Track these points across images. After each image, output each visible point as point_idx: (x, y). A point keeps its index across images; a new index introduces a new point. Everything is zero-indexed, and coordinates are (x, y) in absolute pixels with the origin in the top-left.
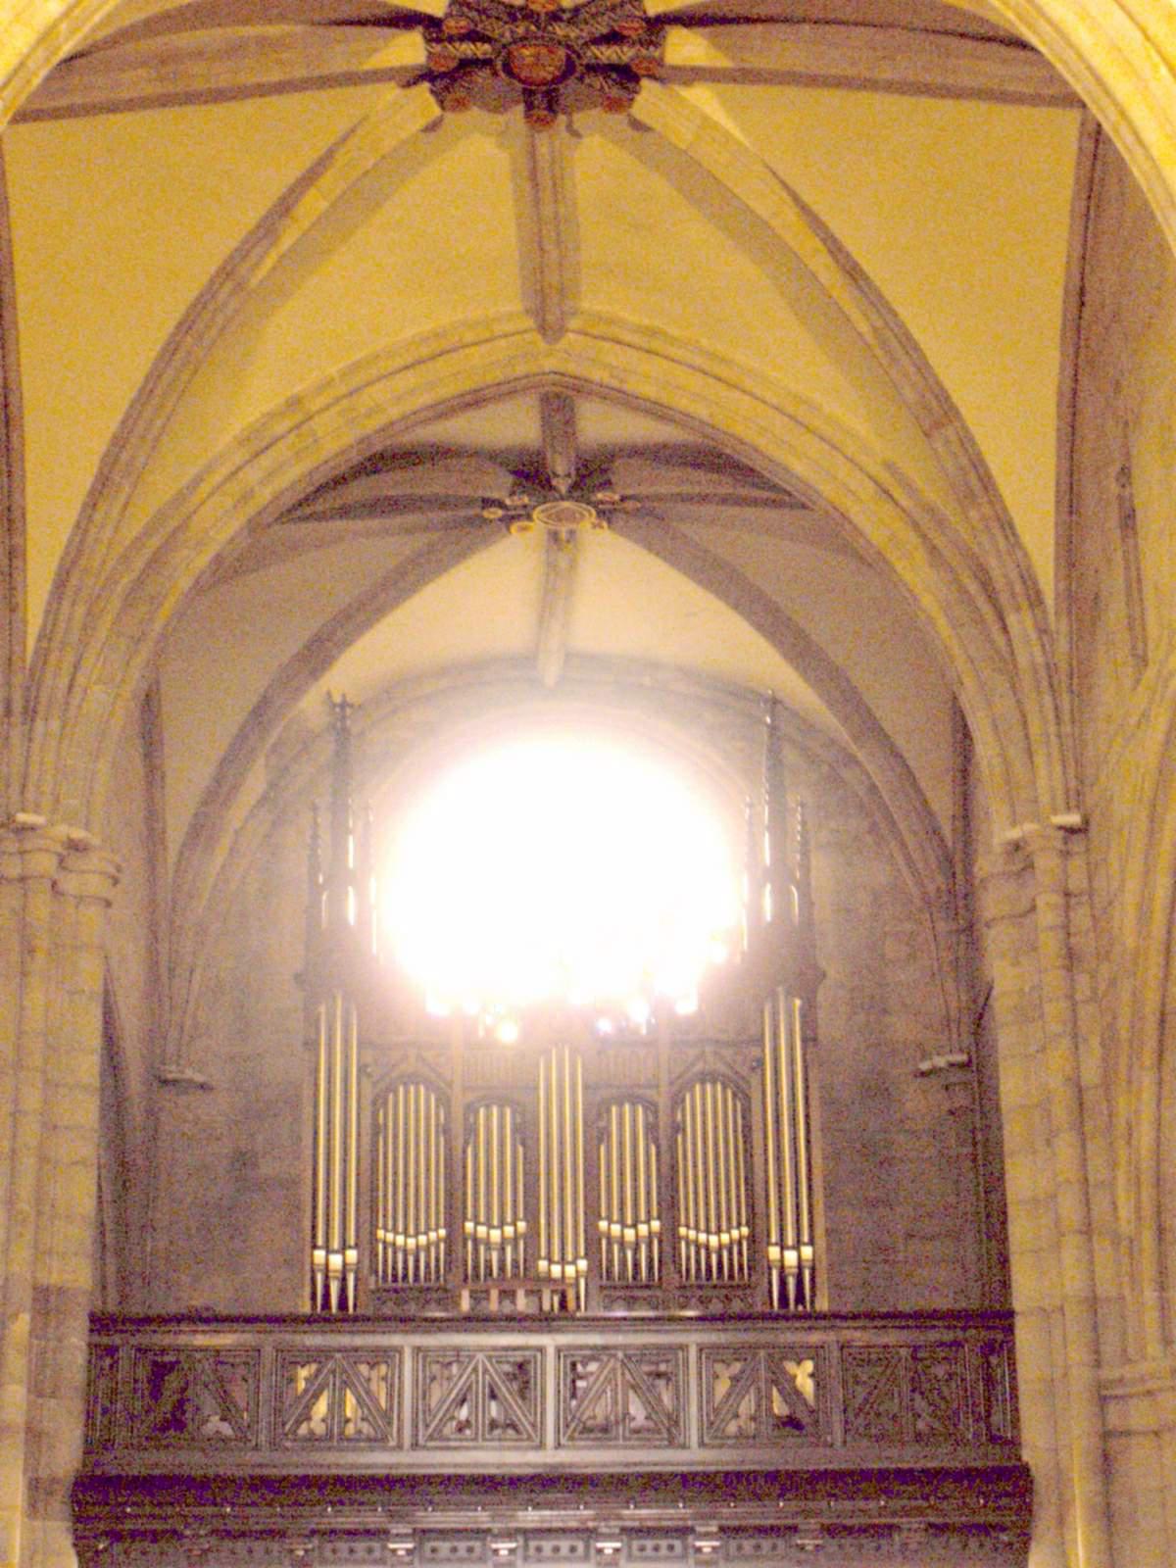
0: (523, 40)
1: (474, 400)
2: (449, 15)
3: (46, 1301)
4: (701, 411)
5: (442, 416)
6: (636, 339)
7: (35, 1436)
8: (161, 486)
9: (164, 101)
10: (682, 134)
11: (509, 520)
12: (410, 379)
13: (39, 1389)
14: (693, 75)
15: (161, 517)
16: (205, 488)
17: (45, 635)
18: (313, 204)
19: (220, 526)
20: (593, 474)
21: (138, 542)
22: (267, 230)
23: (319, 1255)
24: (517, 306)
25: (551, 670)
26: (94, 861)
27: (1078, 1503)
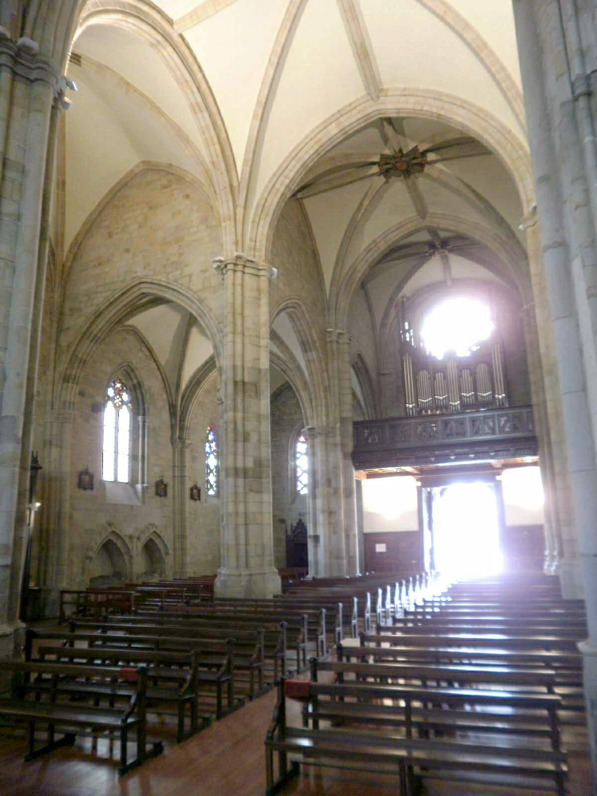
0: (396, 163)
1: (410, 234)
2: (380, 161)
3: (343, 420)
4: (455, 229)
5: (403, 239)
6: (441, 216)
7: (343, 445)
8: (349, 262)
9: (331, 189)
10: (435, 174)
11: (431, 255)
12: (397, 232)
13: (343, 436)
14: (434, 162)
15: (351, 267)
16: (359, 261)
17: (330, 294)
18: (366, 202)
19: (363, 268)
20: (445, 243)
21: (347, 273)
22: (359, 209)
23: (407, 405)
24: (415, 214)
25: (449, 283)
26: (345, 336)
27: (341, 468)
